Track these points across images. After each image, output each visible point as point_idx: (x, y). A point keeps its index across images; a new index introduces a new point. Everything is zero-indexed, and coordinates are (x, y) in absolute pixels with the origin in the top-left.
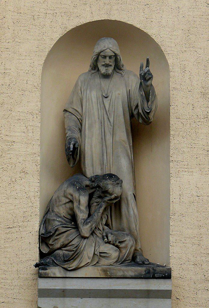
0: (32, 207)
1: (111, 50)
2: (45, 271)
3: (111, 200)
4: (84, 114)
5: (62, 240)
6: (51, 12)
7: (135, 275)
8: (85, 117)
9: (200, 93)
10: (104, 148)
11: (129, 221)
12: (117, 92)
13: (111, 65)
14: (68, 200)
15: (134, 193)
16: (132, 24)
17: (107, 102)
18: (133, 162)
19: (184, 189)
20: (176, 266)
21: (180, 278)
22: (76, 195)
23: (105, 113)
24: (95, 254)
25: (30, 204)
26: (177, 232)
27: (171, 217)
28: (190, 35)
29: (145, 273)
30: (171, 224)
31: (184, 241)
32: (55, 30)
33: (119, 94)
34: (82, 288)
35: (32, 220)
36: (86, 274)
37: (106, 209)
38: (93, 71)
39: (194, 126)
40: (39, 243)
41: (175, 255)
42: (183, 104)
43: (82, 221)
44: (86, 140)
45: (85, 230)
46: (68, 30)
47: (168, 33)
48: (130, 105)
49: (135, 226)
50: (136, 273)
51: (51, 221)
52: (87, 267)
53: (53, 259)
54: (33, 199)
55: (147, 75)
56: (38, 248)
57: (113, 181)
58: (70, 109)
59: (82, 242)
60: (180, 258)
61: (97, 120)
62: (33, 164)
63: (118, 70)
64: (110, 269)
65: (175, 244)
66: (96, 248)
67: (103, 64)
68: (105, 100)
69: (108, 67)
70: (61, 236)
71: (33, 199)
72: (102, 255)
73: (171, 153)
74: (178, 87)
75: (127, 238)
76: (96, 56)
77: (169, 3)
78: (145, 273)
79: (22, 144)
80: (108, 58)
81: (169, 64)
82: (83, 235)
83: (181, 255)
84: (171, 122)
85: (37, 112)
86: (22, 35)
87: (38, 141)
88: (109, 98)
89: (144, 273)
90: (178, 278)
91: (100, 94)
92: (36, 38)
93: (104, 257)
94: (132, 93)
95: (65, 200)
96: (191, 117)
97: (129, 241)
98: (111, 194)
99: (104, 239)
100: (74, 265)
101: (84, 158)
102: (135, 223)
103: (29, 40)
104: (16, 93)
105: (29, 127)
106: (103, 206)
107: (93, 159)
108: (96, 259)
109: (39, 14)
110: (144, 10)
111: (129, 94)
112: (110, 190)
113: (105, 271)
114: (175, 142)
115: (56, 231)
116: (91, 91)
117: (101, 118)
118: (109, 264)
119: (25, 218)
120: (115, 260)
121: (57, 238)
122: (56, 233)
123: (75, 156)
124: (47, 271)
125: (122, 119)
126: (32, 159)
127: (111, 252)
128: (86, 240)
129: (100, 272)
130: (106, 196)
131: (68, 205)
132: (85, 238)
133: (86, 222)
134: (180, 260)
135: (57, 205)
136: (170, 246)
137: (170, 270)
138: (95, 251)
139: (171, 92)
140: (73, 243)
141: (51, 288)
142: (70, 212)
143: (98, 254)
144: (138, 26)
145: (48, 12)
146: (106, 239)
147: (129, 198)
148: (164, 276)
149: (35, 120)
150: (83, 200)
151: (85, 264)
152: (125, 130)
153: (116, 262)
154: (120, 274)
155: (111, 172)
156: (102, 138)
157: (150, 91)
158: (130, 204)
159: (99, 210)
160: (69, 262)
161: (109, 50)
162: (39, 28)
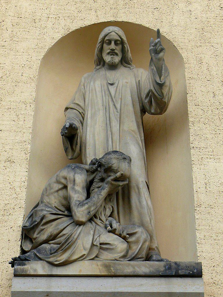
0: (16, 199)
1: (116, 33)
2: (22, 267)
4: (87, 107)
5: (50, 230)
6: (54, 16)
7: (150, 272)
8: (87, 109)
9: (221, 82)
10: (109, 133)
11: (140, 214)
12: (125, 81)
13: (117, 54)
14: (61, 186)
16: (141, 24)
17: (112, 89)
18: (145, 158)
20: (207, 268)
21: (214, 284)
22: (71, 175)
23: (110, 100)
24: (94, 245)
25: (14, 196)
26: (205, 227)
27: (196, 209)
28: (204, 32)
29: (164, 269)
30: (197, 217)
31: (215, 238)
32: (57, 31)
33: (127, 83)
34: (75, 290)
35: (15, 213)
36: (80, 271)
37: (112, 200)
38: (98, 67)
39: (217, 112)
41: (204, 254)
42: (201, 92)
43: (77, 202)
44: (88, 129)
45: (80, 214)
46: (71, 31)
47: (180, 31)
48: (140, 97)
49: (148, 219)
50: (152, 269)
51: (39, 212)
52: (82, 261)
53: (35, 252)
54: (18, 190)
55: (158, 45)
56: (19, 246)
57: (118, 155)
58: (72, 104)
59: (76, 230)
60: (212, 258)
61: (101, 108)
62: (22, 152)
63: (126, 64)
64: (115, 264)
65: (203, 242)
66: (96, 237)
67: (109, 51)
68: (110, 87)
69: (114, 55)
70: (48, 225)
71: (18, 190)
72: (104, 247)
73: (191, 139)
74: (195, 77)
75: (139, 230)
76: (100, 44)
77: (179, 7)
78: (164, 269)
79: (10, 133)
80: (113, 43)
81: (183, 56)
82: (76, 219)
83: (212, 254)
84: (189, 109)
85: (31, 101)
86: (21, 36)
87: (29, 129)
88: (116, 85)
89: (162, 269)
90: (212, 284)
91: (105, 83)
92: (36, 38)
93: (107, 249)
94: (142, 83)
95: (57, 186)
96: (212, 104)
97: (141, 234)
98: (116, 172)
99: (106, 228)
102: (149, 217)
103: (28, 39)
104: (9, 84)
105: (20, 116)
106: (106, 188)
107: (95, 147)
108: (95, 252)
109: (40, 18)
110: (153, 12)
111: (139, 84)
112: (114, 166)
113: (107, 267)
114: (196, 129)
115: (42, 219)
116: (94, 83)
117: (106, 104)
118: (113, 259)
119: (6, 211)
120: (122, 254)
122: (44, 222)
123: (74, 147)
124: (25, 267)
125: (131, 108)
127: (116, 243)
128: (81, 227)
129: (101, 268)
130: (110, 176)
131: (61, 193)
132: (80, 224)
133: (81, 204)
134: (212, 260)
135: (48, 193)
136: (197, 244)
137: (200, 264)
138: (94, 241)
139: (187, 81)
140: (64, 232)
141: (29, 290)
142: (64, 202)
143: (98, 244)
144: (147, 26)
145: (50, 16)
146: (109, 228)
148: (191, 272)
149: (28, 109)
150: (79, 178)
151: (80, 256)
152: (134, 119)
153: (124, 257)
154: (128, 270)
155: (118, 148)
156: (107, 124)
157: (163, 66)
158: (142, 195)
159: (101, 192)
161: (115, 34)
162: (39, 30)
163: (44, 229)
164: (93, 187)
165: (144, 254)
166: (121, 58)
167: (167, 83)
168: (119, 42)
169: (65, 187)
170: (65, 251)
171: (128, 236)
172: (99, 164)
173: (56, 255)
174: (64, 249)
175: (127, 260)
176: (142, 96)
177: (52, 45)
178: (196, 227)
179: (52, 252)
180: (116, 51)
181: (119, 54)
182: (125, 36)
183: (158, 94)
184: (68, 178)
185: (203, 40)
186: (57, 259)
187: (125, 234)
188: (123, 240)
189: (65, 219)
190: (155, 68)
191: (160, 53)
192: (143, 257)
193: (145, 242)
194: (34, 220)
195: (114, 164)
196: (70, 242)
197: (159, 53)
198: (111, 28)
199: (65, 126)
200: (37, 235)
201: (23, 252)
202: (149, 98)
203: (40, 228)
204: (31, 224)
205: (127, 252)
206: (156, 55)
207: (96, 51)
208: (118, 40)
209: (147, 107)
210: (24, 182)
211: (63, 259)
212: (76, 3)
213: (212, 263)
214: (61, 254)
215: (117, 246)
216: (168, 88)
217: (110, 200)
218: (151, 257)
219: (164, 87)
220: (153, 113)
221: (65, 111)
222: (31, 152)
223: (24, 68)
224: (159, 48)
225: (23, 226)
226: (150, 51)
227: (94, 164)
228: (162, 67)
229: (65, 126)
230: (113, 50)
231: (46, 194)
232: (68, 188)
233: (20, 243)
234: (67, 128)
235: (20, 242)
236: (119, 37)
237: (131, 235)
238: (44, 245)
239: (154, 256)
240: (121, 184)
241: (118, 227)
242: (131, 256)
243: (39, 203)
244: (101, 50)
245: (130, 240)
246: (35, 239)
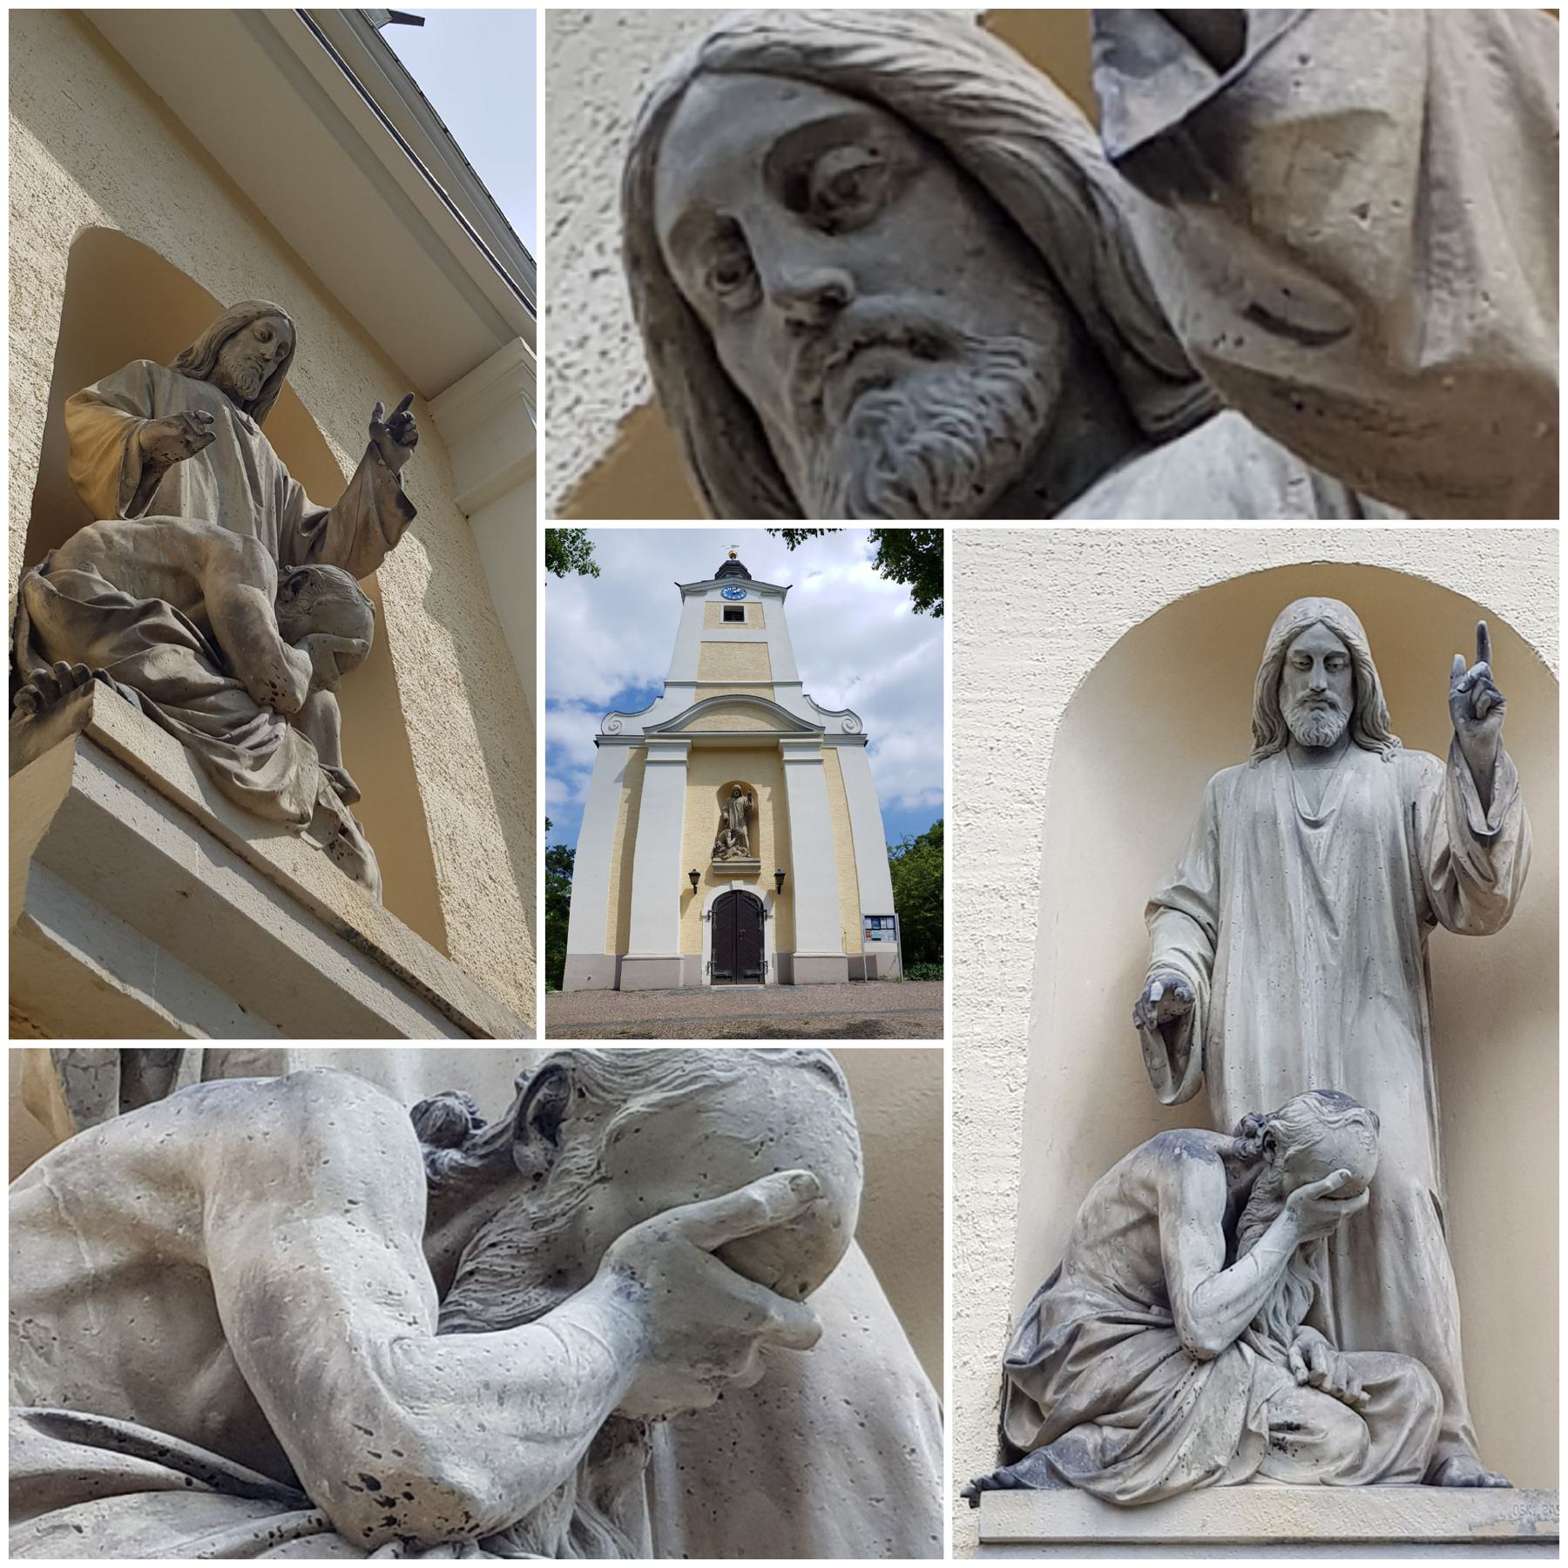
3: (1327, 1197)
5: (1100, 1376)
14: (1134, 1216)
16: (1425, 575)
37: (1312, 1259)
40: (999, 1407)
46: (1164, 602)
53: (1052, 1457)
55: (1480, 687)
67: (1301, 694)
70: (1095, 1360)
80: (1318, 664)
87: (1020, 994)
95: (1122, 1217)
100: (1144, 1479)
101: (1221, 1059)
102: (1441, 1320)
109: (1050, 547)
115: (1072, 1339)
121: (1072, 1369)
123: (1181, 1061)
126: (992, 1063)
127: (1322, 1423)
132: (1202, 1359)
138: (1250, 1418)
140: (1146, 1387)
143: (1265, 1431)
147: (1415, 1210)
153: (1353, 1470)
163: (1080, 1372)
164: (1249, 1217)
165: (1419, 1457)
166: (1348, 716)
167: (1511, 834)
168: (1339, 661)
169: (1150, 1219)
170: (1154, 1454)
171: (1365, 1396)
172: (1268, 1138)
174: (1149, 1449)
176: (1425, 865)
177: (1097, 660)
179: (1111, 1455)
180: (1328, 693)
181: (1340, 705)
182: (1363, 634)
184: (1159, 1189)
186: (1124, 1485)
187: (1356, 1390)
188: (1350, 1412)
189: (1152, 1336)
190: (1468, 774)
192: (1419, 1469)
193: (1428, 1411)
194: (1043, 1340)
197: (1484, 718)
198: (1315, 607)
200: (1056, 1392)
201: (1011, 1454)
204: (1035, 1356)
209: (1441, 905)
211: (1147, 1482)
218: (1444, 1465)
219: (1498, 848)
223: (994, 751)
224: (1484, 697)
226: (1452, 702)
227: (1252, 1135)
231: (1084, 1242)
232: (1162, 1226)
233: (995, 1418)
234: (1154, 1002)
237: (1376, 1391)
238: (1077, 1433)
239: (1456, 1462)
240: (1346, 1208)
241: (1332, 1366)
242: (1376, 1466)
243: (1060, 1267)
244: (1277, 684)
245: (1370, 1409)
246: (1050, 1407)
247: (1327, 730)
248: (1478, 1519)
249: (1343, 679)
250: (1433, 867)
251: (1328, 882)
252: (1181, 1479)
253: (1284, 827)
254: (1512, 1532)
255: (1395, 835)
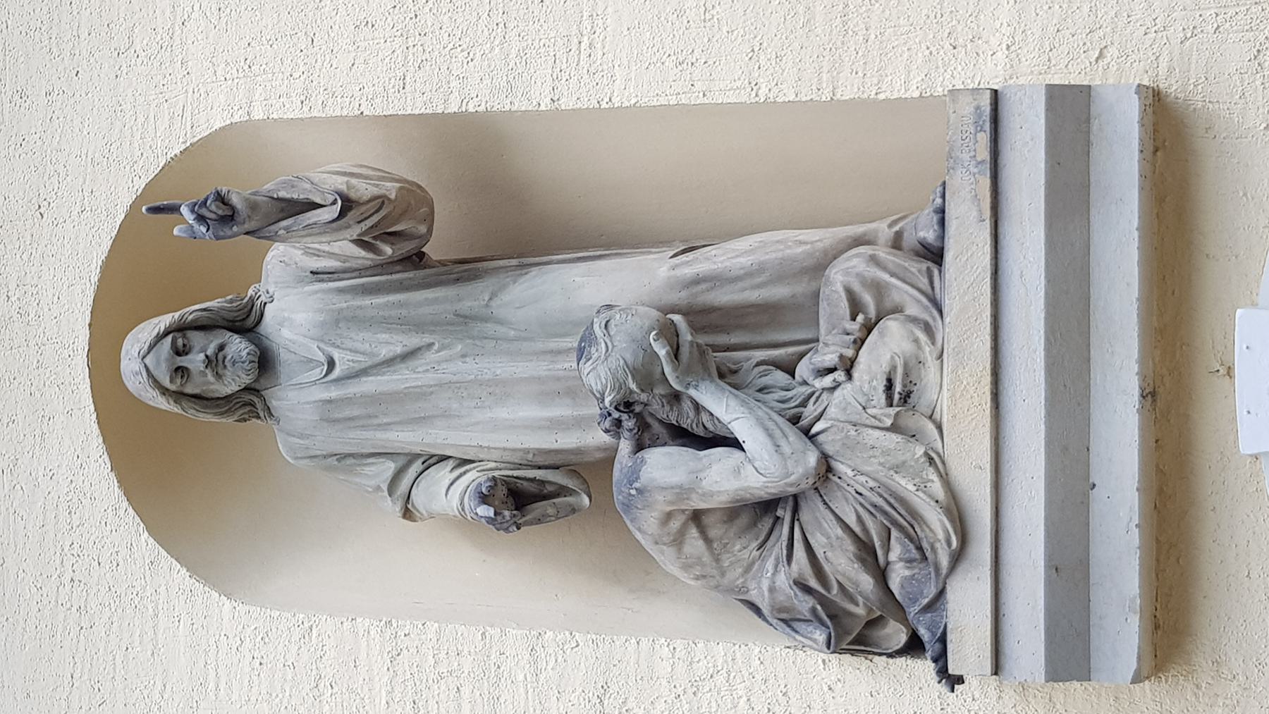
3: (676, 353)
13: (221, 348)
14: (694, 532)
15: (672, 253)
16: (100, 263)
19: (655, 49)
21: (1013, 48)
25: (720, 679)
37: (733, 367)
40: (870, 657)
42: (355, 66)
46: (126, 504)
53: (917, 608)
55: (204, 212)
56: (891, 661)
67: (210, 378)
79: (502, 700)
80: (183, 361)
84: (417, 112)
95: (694, 543)
100: (937, 523)
105: (443, 669)
115: (807, 590)
120: (922, 337)
123: (550, 488)
132: (826, 469)
134: (935, 53)
136: (882, 97)
139: (315, 114)
140: (851, 520)
142: (744, 520)
143: (892, 411)
153: (929, 330)
157: (275, 196)
160: (925, 545)
163: (838, 581)
164: (694, 426)
165: (917, 268)
166: (231, 334)
167: (340, 183)
168: (180, 342)
169: (697, 517)
170: (914, 514)
171: (860, 318)
172: (622, 409)
173: (928, 542)
174: (909, 518)
175: (940, 322)
176: (369, 263)
177: (179, 566)
178: (824, 99)
179: (915, 554)
182: (155, 320)
183: (377, 211)
184: (669, 509)
185: (159, 56)
186: (943, 541)
187: (854, 327)
188: (875, 331)
189: (805, 515)
191: (230, 205)
192: (928, 268)
193: (874, 260)
194: (808, 616)
195: (625, 362)
196: (885, 499)
197: (233, 208)
199: (490, 521)
200: (857, 604)
201: (914, 646)
202: (378, 242)
203: (837, 595)
204: (823, 623)
205: (914, 320)
206: (238, 219)
207: (207, 418)
208: (174, 342)
209: (407, 247)
210: (674, 648)
211: (940, 521)
212: (18, 487)
213: (942, 53)
214: (924, 527)
215: (897, 351)
216: (354, 181)
217: (735, 372)
218: (924, 245)
220: (428, 231)
221: (415, 521)
222: (568, 630)
224: (213, 208)
225: (826, 650)
226: (218, 238)
227: (618, 423)
228: (278, 199)
229: (490, 521)
230: (209, 361)
231: (718, 578)
235: (876, 659)
236: (163, 341)
237: (856, 307)
239: (922, 234)
241: (832, 348)
242: (926, 308)
244: (201, 400)
246: (870, 610)
247: (244, 353)
248: (975, 213)
249: (196, 338)
250: (371, 256)
251: (385, 352)
252: (937, 488)
253: (334, 393)
254: (986, 182)
255: (341, 291)
